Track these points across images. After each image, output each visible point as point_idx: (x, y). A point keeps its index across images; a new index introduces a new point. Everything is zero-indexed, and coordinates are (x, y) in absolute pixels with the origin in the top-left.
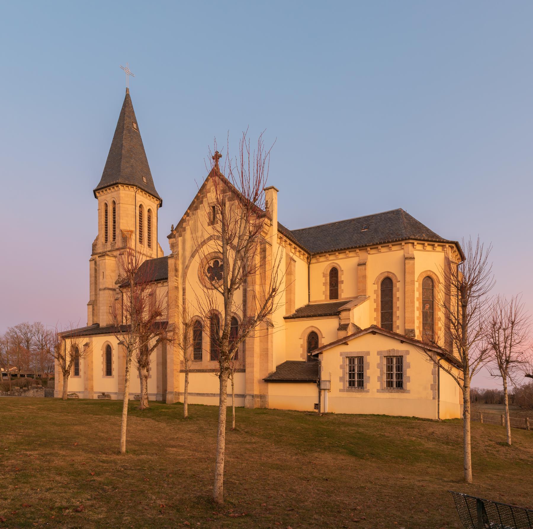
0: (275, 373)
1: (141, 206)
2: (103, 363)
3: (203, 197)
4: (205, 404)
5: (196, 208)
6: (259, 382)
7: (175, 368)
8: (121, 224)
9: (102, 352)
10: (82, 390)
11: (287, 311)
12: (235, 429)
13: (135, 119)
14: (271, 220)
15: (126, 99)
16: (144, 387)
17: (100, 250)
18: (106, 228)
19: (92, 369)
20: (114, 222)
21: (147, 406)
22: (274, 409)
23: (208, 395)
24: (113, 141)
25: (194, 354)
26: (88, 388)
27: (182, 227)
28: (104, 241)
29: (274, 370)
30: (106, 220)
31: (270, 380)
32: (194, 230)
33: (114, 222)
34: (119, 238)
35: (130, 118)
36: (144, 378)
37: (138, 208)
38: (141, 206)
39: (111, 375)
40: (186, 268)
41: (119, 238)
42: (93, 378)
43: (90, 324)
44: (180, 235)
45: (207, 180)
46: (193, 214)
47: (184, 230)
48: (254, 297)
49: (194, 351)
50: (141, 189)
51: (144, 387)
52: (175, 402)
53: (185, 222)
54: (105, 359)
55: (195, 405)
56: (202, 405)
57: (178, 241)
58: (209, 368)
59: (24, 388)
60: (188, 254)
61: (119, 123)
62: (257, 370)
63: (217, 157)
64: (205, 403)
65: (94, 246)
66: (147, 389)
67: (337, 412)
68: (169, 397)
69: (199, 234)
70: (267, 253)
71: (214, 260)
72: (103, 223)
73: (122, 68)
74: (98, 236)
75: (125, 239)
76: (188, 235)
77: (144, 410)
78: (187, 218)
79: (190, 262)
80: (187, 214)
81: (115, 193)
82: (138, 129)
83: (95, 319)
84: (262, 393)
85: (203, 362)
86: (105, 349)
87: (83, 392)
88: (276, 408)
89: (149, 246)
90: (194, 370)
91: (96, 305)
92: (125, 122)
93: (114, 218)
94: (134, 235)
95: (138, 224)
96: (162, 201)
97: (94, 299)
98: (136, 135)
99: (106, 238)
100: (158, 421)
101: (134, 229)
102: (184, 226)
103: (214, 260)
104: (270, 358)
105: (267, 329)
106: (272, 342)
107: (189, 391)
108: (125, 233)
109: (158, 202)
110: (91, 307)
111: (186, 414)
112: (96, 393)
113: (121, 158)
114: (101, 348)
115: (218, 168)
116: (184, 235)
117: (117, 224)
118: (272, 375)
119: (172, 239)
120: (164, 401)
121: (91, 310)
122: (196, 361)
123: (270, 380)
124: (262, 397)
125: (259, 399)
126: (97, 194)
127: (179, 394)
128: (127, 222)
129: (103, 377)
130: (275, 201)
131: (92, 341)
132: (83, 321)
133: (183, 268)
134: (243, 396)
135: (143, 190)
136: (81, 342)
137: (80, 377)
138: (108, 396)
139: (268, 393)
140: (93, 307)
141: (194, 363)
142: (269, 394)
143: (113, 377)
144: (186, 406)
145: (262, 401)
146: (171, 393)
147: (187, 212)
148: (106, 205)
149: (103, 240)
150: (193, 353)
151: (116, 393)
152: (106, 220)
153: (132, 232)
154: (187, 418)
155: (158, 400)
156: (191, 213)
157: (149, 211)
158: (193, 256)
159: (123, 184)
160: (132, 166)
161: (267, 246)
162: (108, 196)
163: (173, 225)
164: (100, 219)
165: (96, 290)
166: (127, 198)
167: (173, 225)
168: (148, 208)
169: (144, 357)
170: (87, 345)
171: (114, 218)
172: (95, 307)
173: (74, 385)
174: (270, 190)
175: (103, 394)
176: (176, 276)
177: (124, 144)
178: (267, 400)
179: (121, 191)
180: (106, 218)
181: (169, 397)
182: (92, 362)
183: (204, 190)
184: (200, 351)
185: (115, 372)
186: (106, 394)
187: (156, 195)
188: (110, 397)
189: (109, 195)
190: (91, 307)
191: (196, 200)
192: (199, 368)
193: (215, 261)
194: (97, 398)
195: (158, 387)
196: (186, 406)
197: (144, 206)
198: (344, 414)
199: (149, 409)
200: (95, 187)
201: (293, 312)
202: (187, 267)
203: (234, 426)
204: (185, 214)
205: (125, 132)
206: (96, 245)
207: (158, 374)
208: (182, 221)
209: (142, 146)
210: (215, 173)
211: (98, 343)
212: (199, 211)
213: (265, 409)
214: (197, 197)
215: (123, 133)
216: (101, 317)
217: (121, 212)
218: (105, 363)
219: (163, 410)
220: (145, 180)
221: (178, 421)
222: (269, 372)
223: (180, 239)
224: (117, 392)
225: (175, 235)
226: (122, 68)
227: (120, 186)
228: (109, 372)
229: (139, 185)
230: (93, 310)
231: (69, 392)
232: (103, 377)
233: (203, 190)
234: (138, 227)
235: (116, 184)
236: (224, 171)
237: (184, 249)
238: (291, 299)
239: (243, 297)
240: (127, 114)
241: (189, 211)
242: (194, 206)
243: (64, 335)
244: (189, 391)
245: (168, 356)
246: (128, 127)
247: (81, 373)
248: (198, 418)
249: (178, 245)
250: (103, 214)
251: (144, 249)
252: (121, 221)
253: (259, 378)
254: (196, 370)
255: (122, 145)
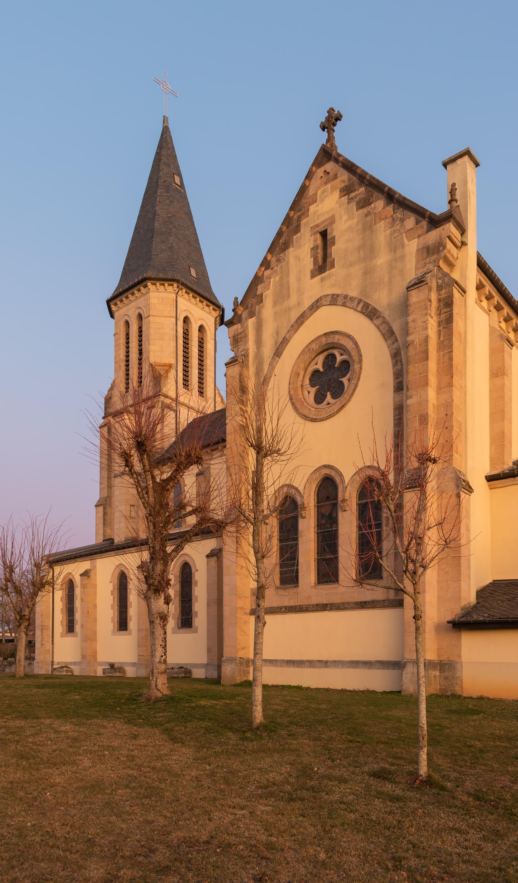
0: (475, 606)
1: (186, 320)
2: (113, 607)
3: (299, 219)
4: (305, 685)
5: (286, 246)
6: (438, 628)
7: (240, 604)
8: (151, 354)
9: (111, 587)
10: (78, 659)
11: (493, 461)
12: (429, 782)
13: (177, 168)
14: (463, 231)
15: (162, 135)
16: (159, 642)
17: (118, 404)
18: (127, 365)
19: (95, 620)
20: (141, 353)
21: (166, 692)
22: (481, 698)
23: (311, 664)
24: (140, 211)
25: (281, 573)
26: (88, 655)
27: (255, 295)
28: (123, 390)
29: (472, 599)
30: (128, 352)
31: (465, 623)
32: (282, 294)
33: (141, 353)
34: (147, 381)
35: (169, 166)
36: (158, 621)
37: (180, 323)
38: (186, 320)
39: (126, 630)
40: (263, 382)
41: (147, 381)
42: (92, 636)
43: (101, 539)
44: (252, 315)
45: (309, 176)
46: (278, 261)
47: (260, 299)
48: (424, 419)
49: (281, 567)
50: (186, 287)
51: (159, 642)
52: (239, 679)
53: (262, 282)
54: (116, 599)
55: (283, 687)
56: (299, 688)
57: (247, 328)
58: (314, 601)
59: (9, 659)
60: (268, 351)
61: (150, 178)
62: (437, 598)
63: (331, 121)
64: (305, 684)
65: (108, 400)
66: (165, 647)
67: (313, 686)
68: (227, 670)
69: (293, 299)
70: (456, 310)
71: (325, 354)
72: (123, 357)
73: (156, 81)
74: (114, 381)
75: (158, 380)
76: (268, 310)
77: (157, 700)
78: (267, 273)
79: (272, 367)
80: (265, 264)
81: (142, 299)
82: (182, 185)
83: (108, 531)
84: (444, 658)
85: (300, 589)
86: (116, 581)
87: (79, 663)
88: (485, 694)
89: (201, 393)
90: (281, 608)
91: (110, 506)
92: (161, 174)
93: (140, 345)
94: (173, 372)
95: (181, 353)
96: (223, 310)
97: (106, 495)
98: (180, 195)
99: (127, 384)
100: (174, 740)
101: (173, 361)
102: (259, 292)
103: (325, 354)
104: (463, 569)
105: (458, 496)
106: (468, 529)
107: (267, 654)
108: (158, 368)
109: (216, 314)
110: (101, 509)
111: (258, 715)
112: (101, 664)
113: (153, 237)
114: (109, 578)
115: (333, 146)
116: (260, 312)
117: (144, 356)
118: (469, 611)
119: (235, 327)
120: (217, 681)
121: (101, 514)
122: (285, 589)
123: (465, 623)
124: (446, 667)
125: (437, 673)
126: (113, 308)
127: (247, 662)
128: (162, 349)
129: (113, 634)
130: (472, 187)
131: (94, 567)
132: (90, 538)
133: (256, 386)
134: (398, 665)
135: (190, 289)
136: (75, 569)
137: (76, 636)
138: (121, 669)
139: (460, 656)
140: (105, 509)
141: (281, 592)
142: (464, 659)
143: (130, 634)
144: (258, 693)
145: (446, 678)
146: (232, 660)
147: (265, 258)
148: (127, 323)
149: (122, 387)
150: (278, 570)
151: (134, 664)
152: (128, 352)
153: (170, 366)
154: (263, 727)
155: (209, 676)
156: (274, 260)
157: (201, 329)
158: (278, 353)
159: (155, 280)
160: (171, 248)
161: (456, 293)
162: (128, 309)
163: (236, 299)
164: (116, 351)
165: (109, 478)
166: (164, 305)
167: (236, 299)
168: (199, 324)
169: (159, 567)
170: (86, 574)
171: (140, 345)
172: (108, 510)
173: (62, 651)
174: (459, 161)
175: (112, 666)
176: (242, 402)
177: (159, 212)
178: (458, 674)
179: (151, 294)
180: (128, 347)
181: (228, 670)
182: (95, 606)
183: (303, 201)
184: (293, 565)
185: (132, 624)
186: (116, 666)
187: (212, 299)
188: (124, 672)
189: (133, 305)
190: (101, 509)
191: (284, 228)
192: (291, 603)
193: (327, 357)
194: (102, 675)
195: (209, 651)
196: (258, 693)
197: (192, 320)
198: (316, 689)
199: (169, 700)
200: (109, 294)
201: (508, 465)
202: (266, 381)
203: (423, 770)
204: (261, 265)
205: (159, 191)
206: (110, 398)
207: (209, 624)
208: (257, 280)
209: (189, 214)
210: (327, 154)
211: (106, 568)
212: (291, 249)
213: (454, 696)
214: (287, 221)
215: (156, 192)
216: (116, 526)
217: (152, 331)
218: (116, 607)
219: (203, 702)
220: (193, 273)
221: (233, 737)
222: (464, 603)
223: (251, 322)
224: (136, 661)
225: (241, 316)
226: (156, 81)
227: (149, 284)
228: (123, 624)
229: (183, 280)
230: (105, 514)
231: (59, 663)
232: (113, 634)
233: (300, 203)
234: (181, 358)
235: (143, 281)
236: (346, 146)
237: (259, 343)
238: (503, 433)
239: (395, 425)
240: (164, 159)
241: (269, 258)
242: (280, 244)
243: (51, 559)
244: (267, 654)
245: (226, 580)
246: (165, 182)
247: (78, 628)
248: (293, 728)
249: (246, 336)
250: (123, 340)
251: (190, 397)
252: (152, 348)
253: (436, 620)
254: (286, 607)
255: (155, 214)
